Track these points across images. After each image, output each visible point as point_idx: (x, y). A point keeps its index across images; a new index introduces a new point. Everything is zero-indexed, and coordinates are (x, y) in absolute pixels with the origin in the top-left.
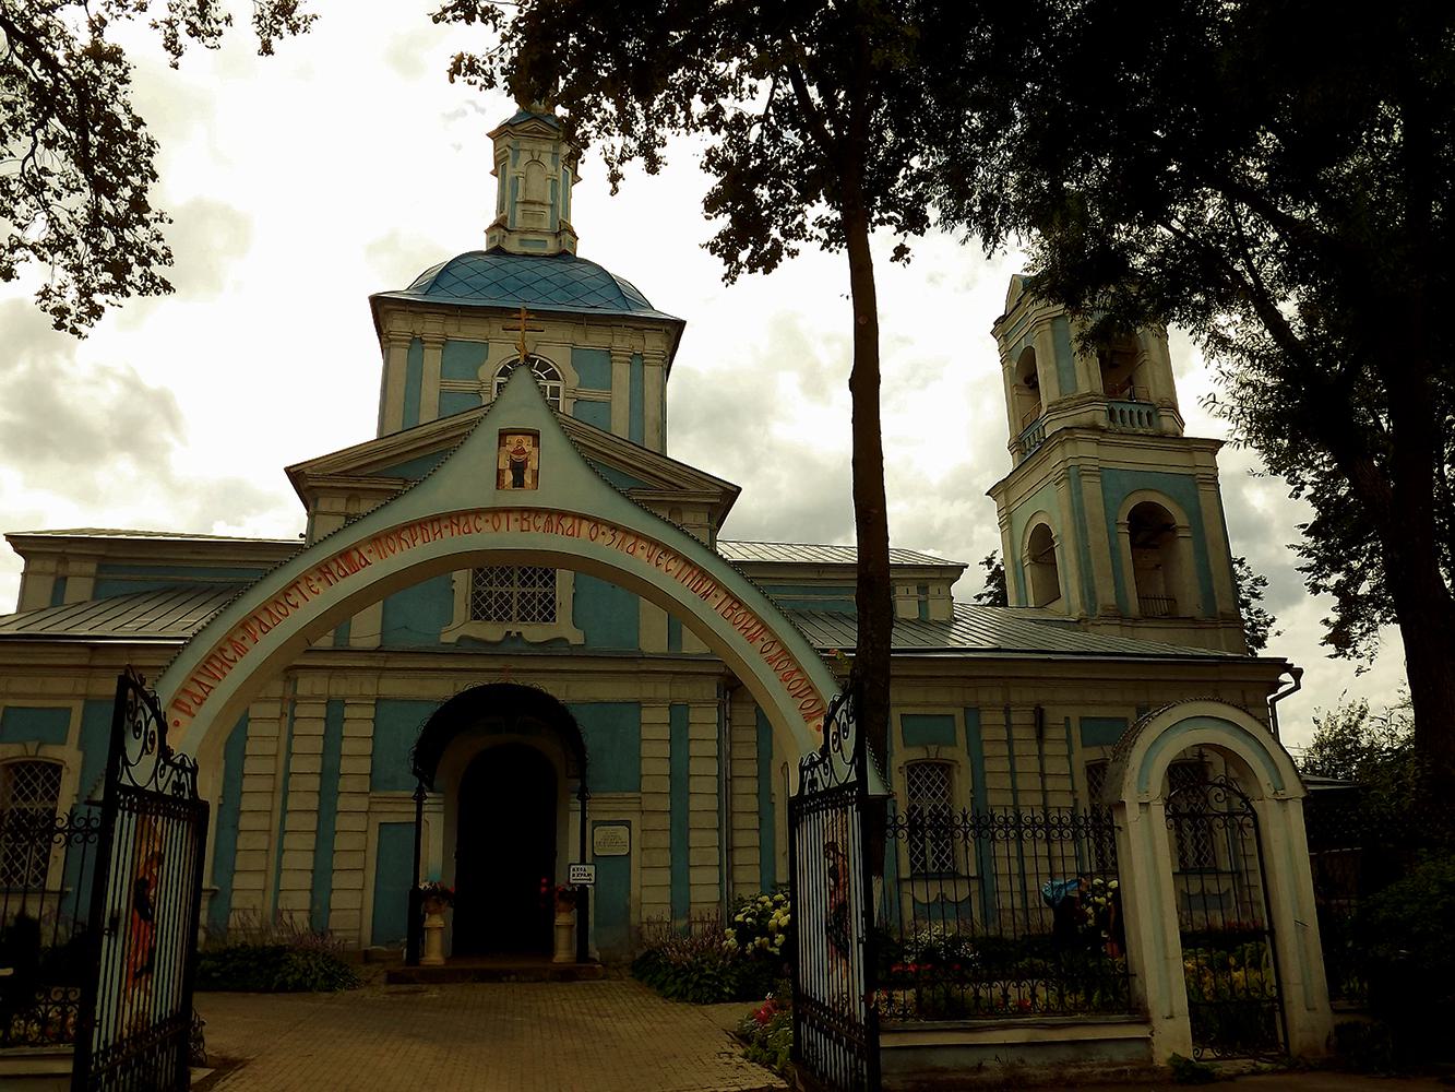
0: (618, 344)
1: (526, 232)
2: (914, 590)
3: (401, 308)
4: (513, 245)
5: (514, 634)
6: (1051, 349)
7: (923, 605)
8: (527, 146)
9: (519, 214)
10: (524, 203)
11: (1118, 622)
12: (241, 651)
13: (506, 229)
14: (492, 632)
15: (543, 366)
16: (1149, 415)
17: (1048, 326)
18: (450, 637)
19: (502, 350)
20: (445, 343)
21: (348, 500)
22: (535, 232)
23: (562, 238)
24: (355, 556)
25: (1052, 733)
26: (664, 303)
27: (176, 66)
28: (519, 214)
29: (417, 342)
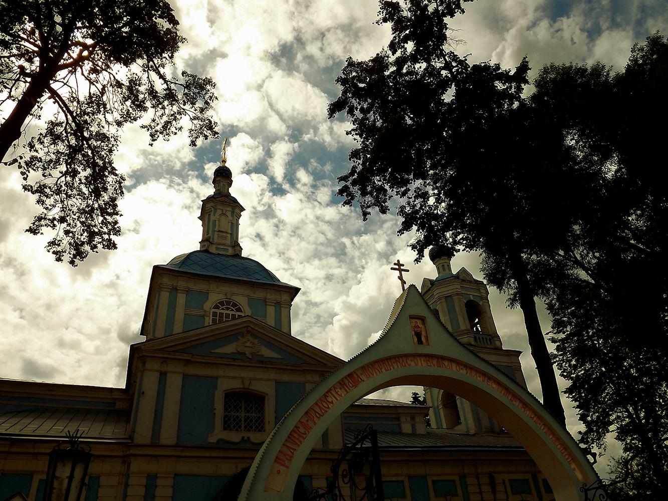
0: (269, 296)
1: (219, 244)
2: (409, 419)
3: (169, 273)
4: (213, 249)
5: (246, 438)
6: (446, 310)
7: (413, 426)
8: (221, 207)
9: (216, 236)
10: (219, 231)
11: (492, 435)
12: (308, 429)
13: (210, 242)
14: (234, 437)
15: (235, 305)
16: (490, 340)
17: (444, 300)
18: (213, 439)
19: (215, 297)
20: (188, 291)
21: (162, 363)
22: (223, 244)
23: (236, 248)
24: (355, 375)
25: (500, 488)
26: (285, 278)
27: (151, 145)
28: (216, 236)
29: (174, 290)
